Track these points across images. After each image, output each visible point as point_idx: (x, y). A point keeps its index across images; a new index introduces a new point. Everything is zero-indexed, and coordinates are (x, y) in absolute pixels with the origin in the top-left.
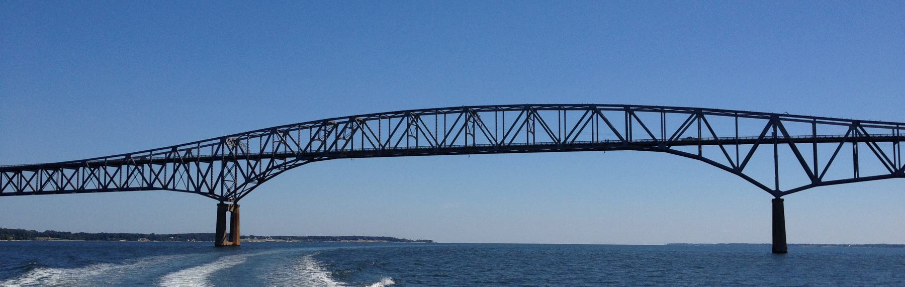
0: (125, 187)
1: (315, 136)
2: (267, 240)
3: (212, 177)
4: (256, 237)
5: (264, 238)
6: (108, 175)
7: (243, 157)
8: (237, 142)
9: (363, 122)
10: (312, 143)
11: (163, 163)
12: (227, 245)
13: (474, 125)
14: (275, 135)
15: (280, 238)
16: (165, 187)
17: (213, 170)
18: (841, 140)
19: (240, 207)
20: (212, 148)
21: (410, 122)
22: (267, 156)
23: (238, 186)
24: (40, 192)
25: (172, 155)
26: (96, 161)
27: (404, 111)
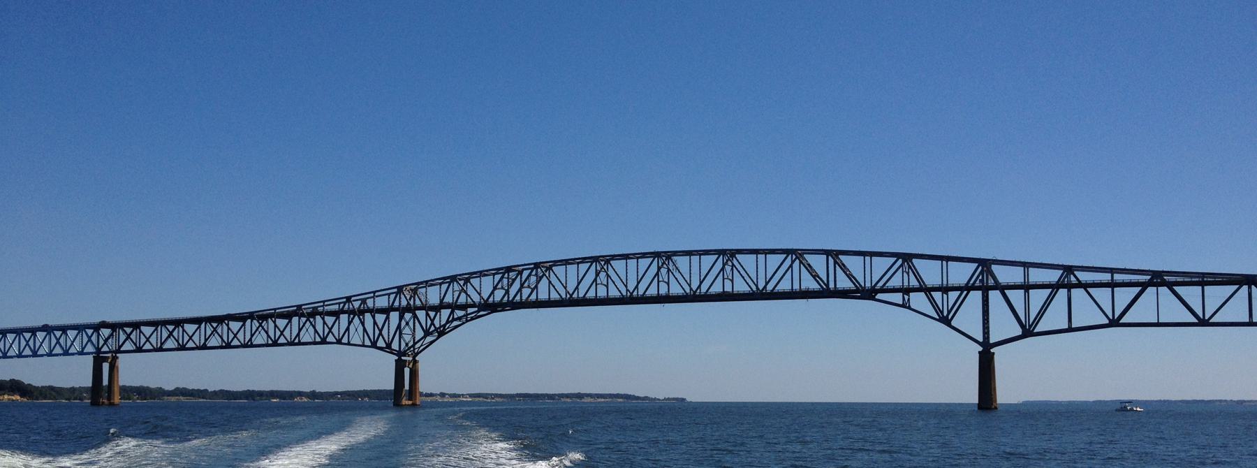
2: (461, 399)
4: (447, 394)
5: (459, 396)
8: (415, 291)
10: (495, 292)
11: (336, 314)
13: (732, 269)
15: (479, 395)
16: (339, 342)
19: (419, 364)
20: (389, 298)
22: (448, 306)
24: (160, 349)
25: (347, 306)
26: (265, 313)
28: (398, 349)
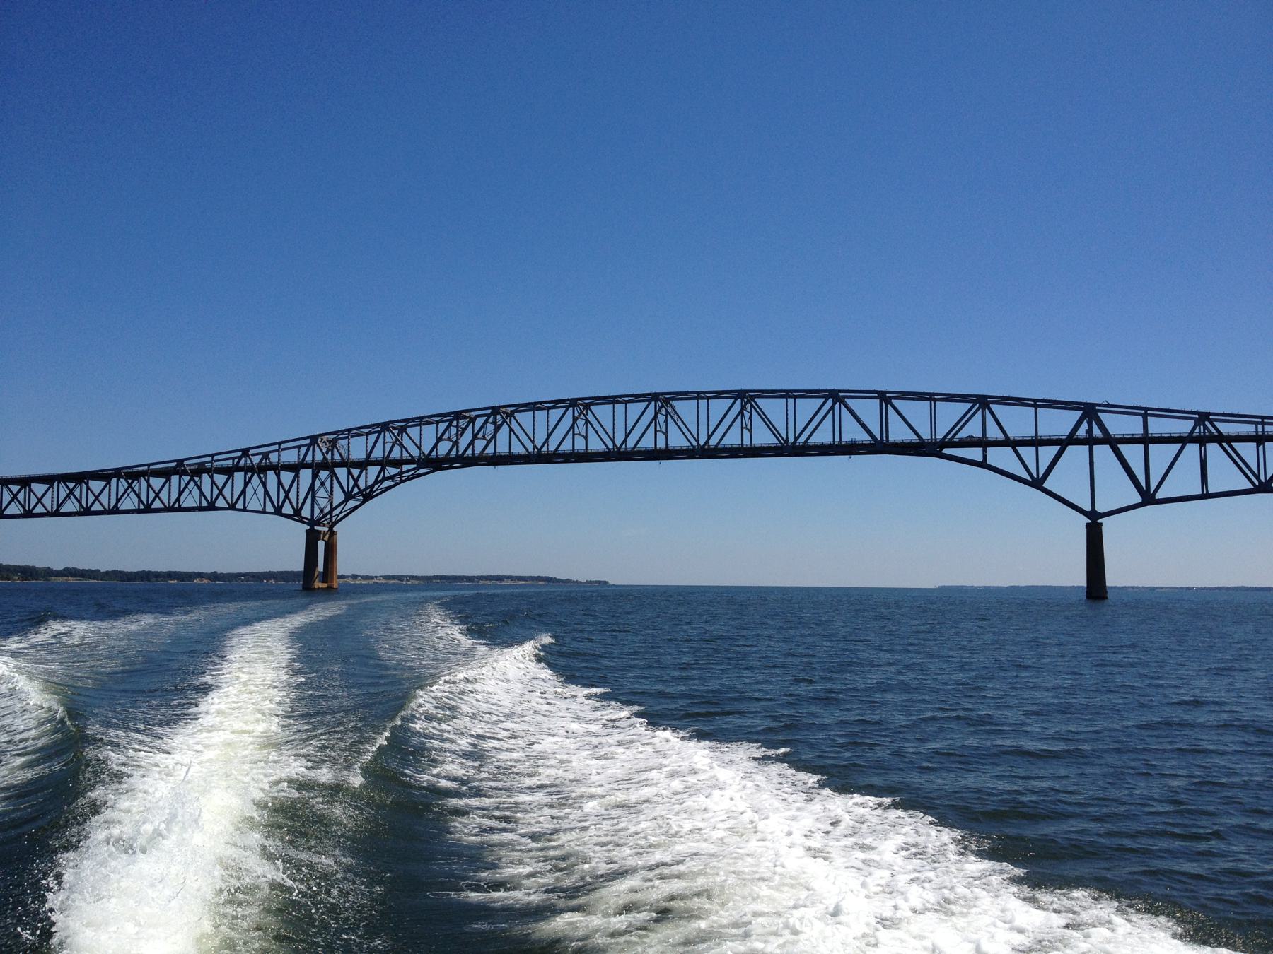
0: (176, 506)
1: (443, 435)
2: (375, 581)
3: (298, 492)
5: (372, 578)
6: (152, 489)
7: (343, 464)
8: (333, 443)
9: (511, 415)
10: (439, 444)
11: (229, 472)
12: (319, 589)
14: (387, 433)
15: (394, 577)
16: (232, 507)
17: (300, 483)
18: (1183, 440)
20: (299, 452)
21: (576, 414)
22: (375, 463)
23: (334, 505)
24: (57, 514)
25: (242, 462)
26: (135, 469)
27: (568, 400)
28: (309, 517)
